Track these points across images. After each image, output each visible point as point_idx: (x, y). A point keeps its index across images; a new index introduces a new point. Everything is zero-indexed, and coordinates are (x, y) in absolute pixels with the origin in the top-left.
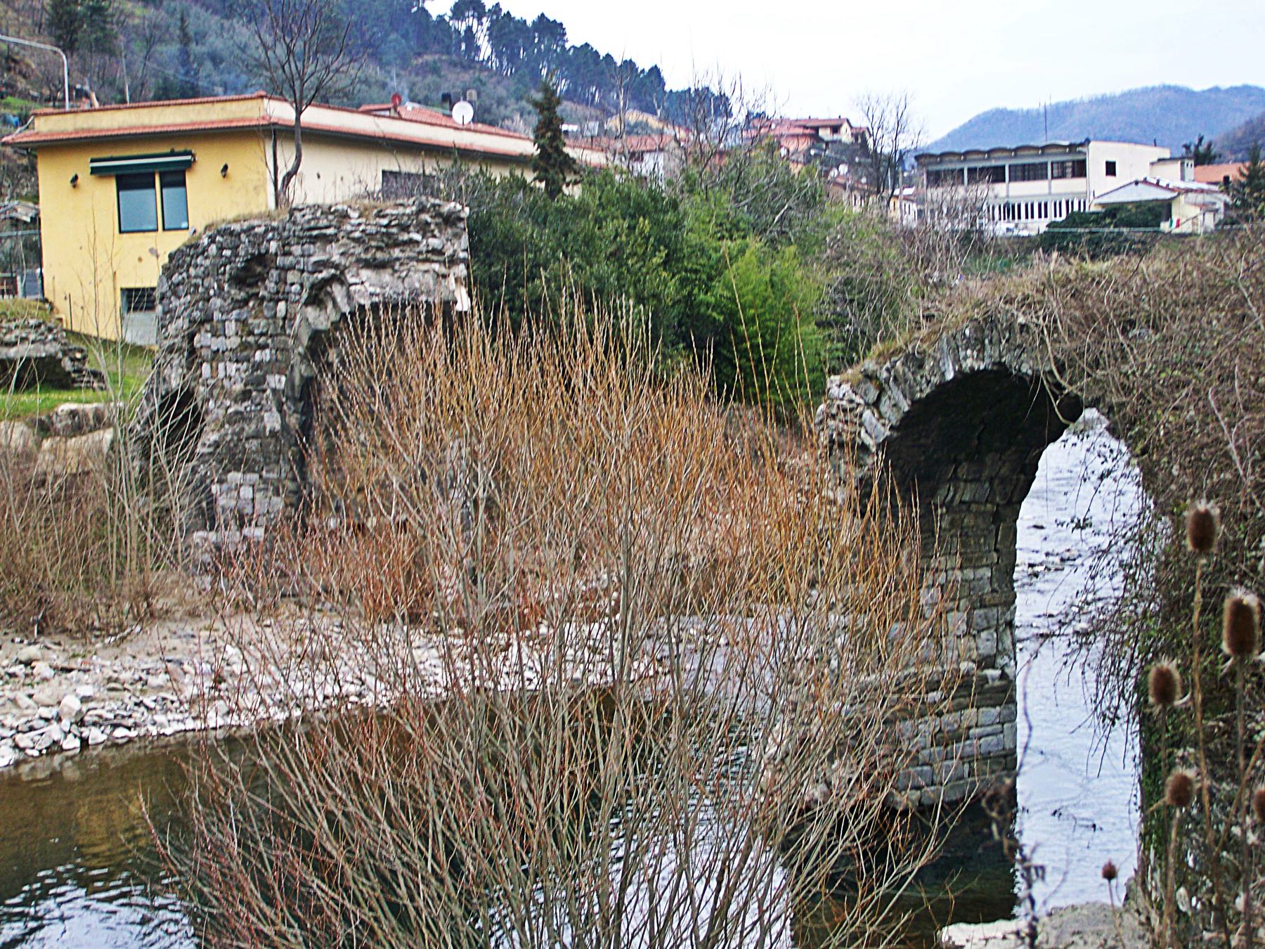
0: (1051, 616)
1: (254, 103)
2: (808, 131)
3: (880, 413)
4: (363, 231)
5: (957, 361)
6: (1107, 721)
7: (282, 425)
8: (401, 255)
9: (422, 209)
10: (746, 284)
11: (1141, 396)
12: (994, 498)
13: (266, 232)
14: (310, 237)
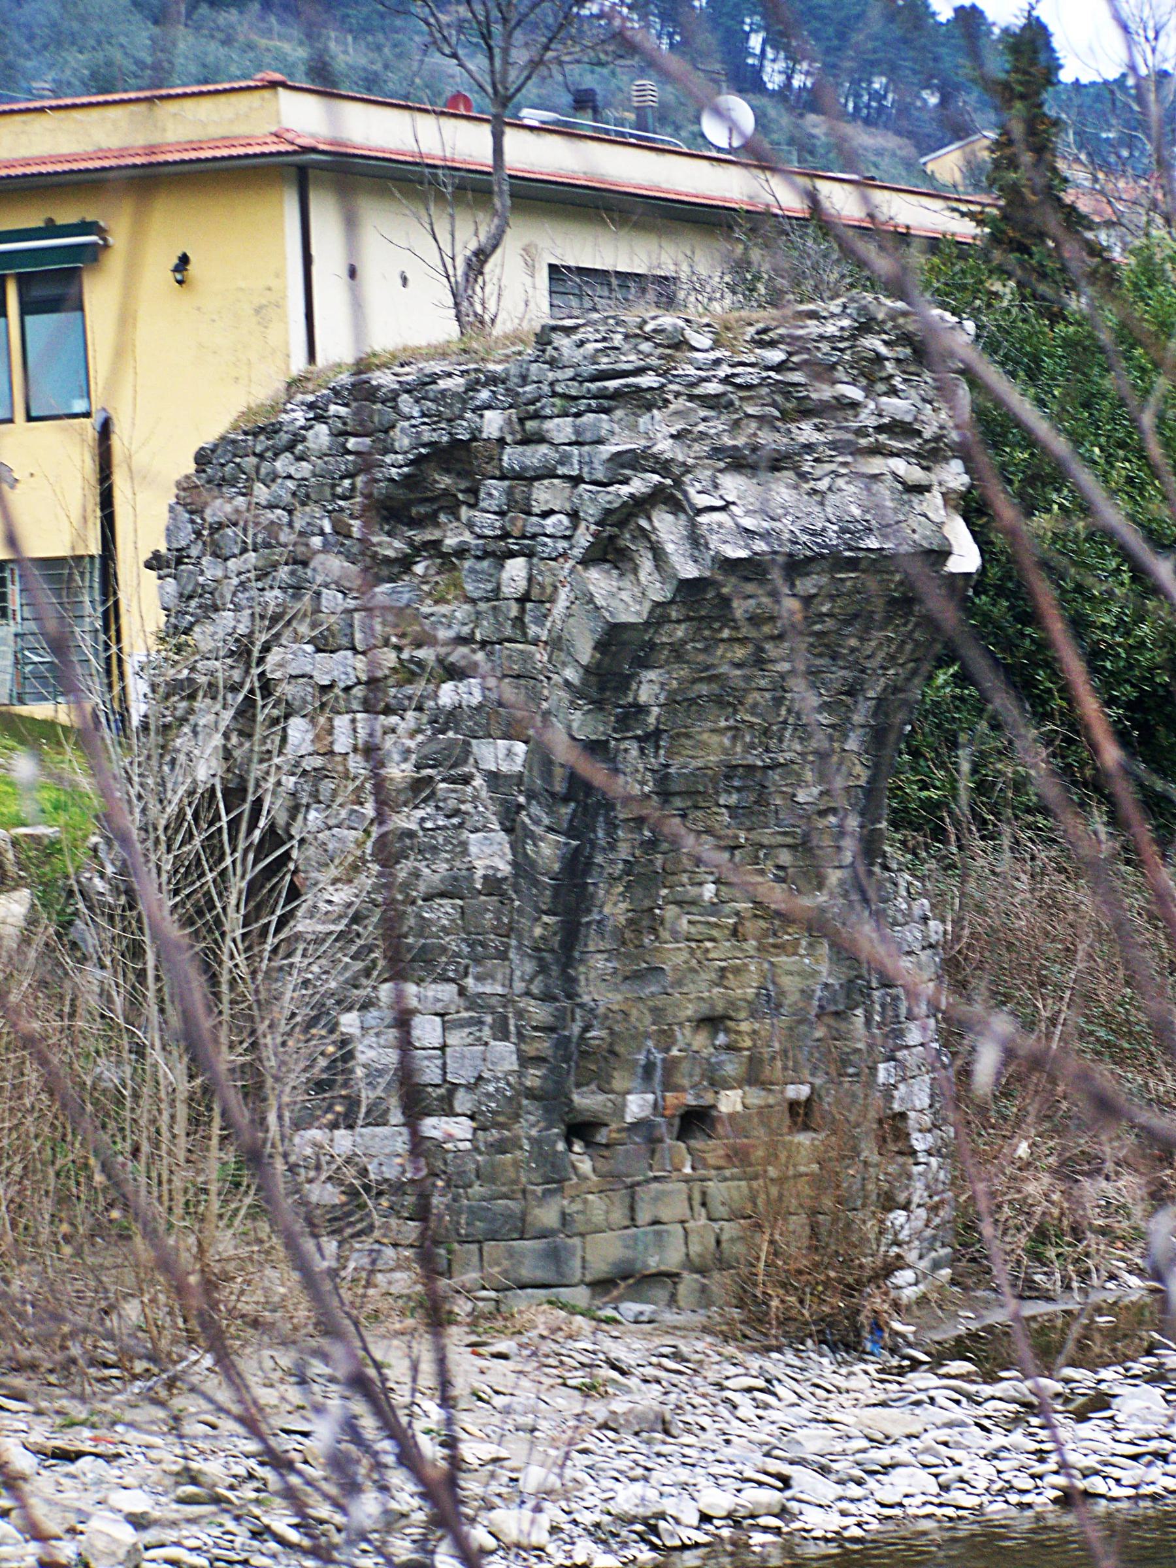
1: (254, 99)
4: (726, 380)
7: (514, 864)
8: (816, 437)
9: (866, 326)
13: (472, 387)
14: (601, 395)
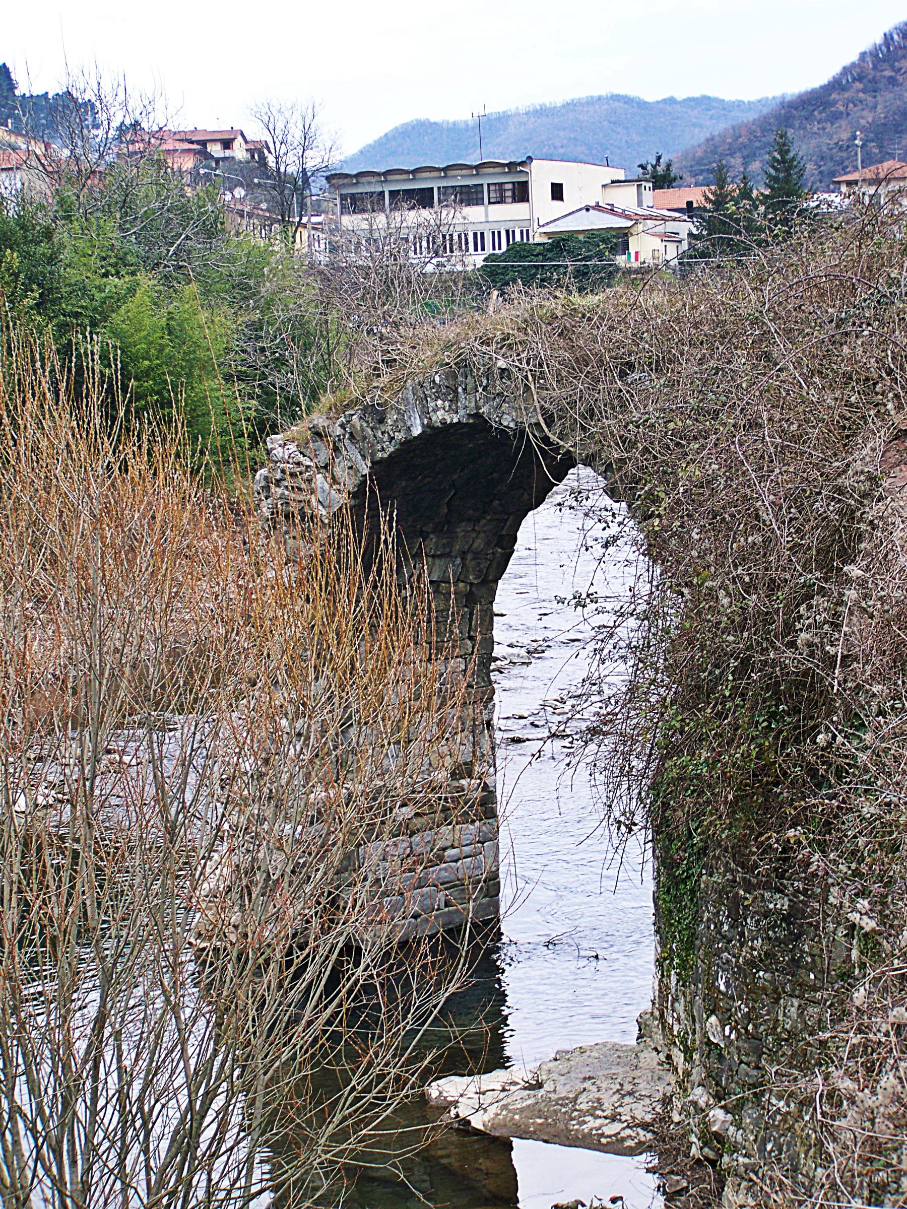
0: (521, 717)
2: (195, 146)
3: (333, 478)
5: (425, 413)
6: (623, 828)
10: (138, 330)
11: (646, 450)
12: (467, 577)
